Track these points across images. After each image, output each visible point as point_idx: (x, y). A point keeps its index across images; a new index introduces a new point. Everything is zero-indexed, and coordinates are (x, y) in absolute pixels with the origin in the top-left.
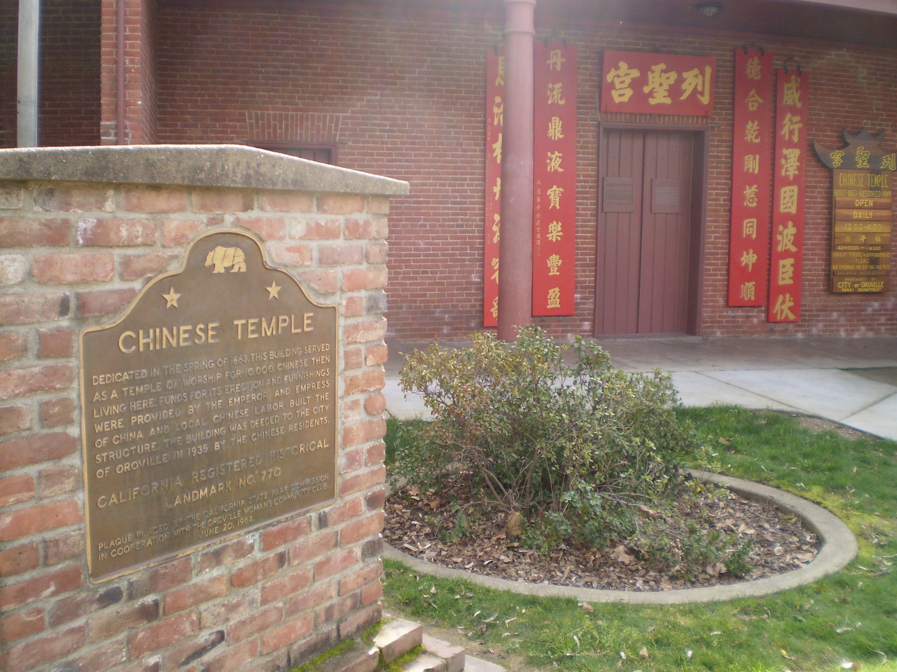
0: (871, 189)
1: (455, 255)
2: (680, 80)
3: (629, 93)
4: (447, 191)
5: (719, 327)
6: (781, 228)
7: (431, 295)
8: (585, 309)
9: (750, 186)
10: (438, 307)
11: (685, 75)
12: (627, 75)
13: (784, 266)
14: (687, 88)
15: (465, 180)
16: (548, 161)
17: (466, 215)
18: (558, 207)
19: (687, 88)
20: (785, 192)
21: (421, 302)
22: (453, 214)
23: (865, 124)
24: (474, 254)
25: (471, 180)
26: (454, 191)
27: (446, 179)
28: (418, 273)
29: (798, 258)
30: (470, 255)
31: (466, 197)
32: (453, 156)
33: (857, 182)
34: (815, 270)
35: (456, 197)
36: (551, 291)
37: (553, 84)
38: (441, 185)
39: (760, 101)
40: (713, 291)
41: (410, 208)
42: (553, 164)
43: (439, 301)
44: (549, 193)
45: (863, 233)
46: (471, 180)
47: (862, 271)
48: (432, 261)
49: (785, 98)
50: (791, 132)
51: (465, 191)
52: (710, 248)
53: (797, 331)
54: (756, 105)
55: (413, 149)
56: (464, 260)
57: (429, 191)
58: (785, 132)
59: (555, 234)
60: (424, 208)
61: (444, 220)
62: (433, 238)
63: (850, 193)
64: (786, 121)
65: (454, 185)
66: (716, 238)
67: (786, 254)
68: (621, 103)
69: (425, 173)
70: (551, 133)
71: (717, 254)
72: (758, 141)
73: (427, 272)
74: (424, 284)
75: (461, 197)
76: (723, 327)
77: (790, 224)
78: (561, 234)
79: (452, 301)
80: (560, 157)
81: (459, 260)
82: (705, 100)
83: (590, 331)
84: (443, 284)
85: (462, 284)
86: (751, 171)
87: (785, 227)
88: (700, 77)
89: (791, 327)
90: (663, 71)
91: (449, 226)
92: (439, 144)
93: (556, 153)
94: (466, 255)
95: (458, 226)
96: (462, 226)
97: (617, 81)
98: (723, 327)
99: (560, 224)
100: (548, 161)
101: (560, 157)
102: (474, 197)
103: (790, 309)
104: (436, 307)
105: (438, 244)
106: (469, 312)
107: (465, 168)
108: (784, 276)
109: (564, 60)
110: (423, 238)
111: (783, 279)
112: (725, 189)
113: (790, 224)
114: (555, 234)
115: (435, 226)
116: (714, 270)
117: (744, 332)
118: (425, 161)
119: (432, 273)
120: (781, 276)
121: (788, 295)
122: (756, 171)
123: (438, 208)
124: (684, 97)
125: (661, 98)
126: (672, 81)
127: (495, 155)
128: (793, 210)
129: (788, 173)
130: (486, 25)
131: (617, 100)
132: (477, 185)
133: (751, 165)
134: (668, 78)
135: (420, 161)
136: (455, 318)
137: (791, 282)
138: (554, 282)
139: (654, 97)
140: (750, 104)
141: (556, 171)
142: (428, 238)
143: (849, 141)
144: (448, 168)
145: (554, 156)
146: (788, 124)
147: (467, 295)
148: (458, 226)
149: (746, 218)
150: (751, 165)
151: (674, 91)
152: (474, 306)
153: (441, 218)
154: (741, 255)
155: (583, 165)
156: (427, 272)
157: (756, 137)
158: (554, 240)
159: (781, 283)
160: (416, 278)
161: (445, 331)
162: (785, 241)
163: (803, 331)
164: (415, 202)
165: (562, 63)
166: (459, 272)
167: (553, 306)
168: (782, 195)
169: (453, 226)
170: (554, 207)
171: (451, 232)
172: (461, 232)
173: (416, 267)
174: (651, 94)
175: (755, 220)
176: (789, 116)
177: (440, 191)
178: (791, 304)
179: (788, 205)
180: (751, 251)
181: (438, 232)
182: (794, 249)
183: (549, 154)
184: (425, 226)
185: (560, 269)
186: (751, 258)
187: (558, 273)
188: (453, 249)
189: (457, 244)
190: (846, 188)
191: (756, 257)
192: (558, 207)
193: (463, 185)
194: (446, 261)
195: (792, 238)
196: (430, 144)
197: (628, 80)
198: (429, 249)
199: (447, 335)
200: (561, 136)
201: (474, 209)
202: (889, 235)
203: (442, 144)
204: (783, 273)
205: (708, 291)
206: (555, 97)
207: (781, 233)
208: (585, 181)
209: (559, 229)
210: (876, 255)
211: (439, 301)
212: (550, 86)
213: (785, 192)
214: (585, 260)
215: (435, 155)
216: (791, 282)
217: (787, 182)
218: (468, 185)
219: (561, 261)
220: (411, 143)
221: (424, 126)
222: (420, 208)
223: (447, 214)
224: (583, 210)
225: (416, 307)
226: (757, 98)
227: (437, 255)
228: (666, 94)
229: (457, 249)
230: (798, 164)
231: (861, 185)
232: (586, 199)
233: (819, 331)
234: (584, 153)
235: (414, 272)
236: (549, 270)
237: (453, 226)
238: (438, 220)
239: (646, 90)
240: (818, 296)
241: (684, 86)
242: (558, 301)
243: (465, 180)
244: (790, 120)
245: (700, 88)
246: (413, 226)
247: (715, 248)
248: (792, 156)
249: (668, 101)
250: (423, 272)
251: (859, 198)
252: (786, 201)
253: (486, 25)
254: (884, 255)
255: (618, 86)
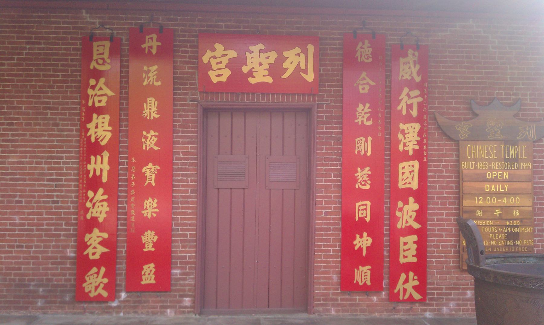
0: (506, 160)
1: (50, 230)
2: (281, 59)
3: (227, 73)
4: (43, 169)
5: (333, 305)
6: (400, 204)
7: (26, 269)
8: (185, 285)
9: (362, 169)
10: (33, 280)
11: (285, 54)
12: (223, 56)
13: (405, 244)
14: (290, 67)
15: (62, 158)
16: (143, 140)
17: (62, 191)
18: (154, 184)
19: (290, 67)
20: (404, 168)
21: (15, 275)
22: (48, 191)
23: (497, 94)
24: (70, 230)
25: (67, 158)
26: (49, 169)
27: (43, 158)
28: (13, 247)
29: (422, 236)
30: (65, 230)
31: (61, 175)
32: (49, 135)
33: (488, 154)
34: (443, 246)
35: (51, 175)
36: (145, 267)
37: (148, 67)
38: (37, 163)
39: (373, 83)
40: (325, 267)
41: (6, 185)
42: (148, 143)
43: (34, 275)
44: (144, 170)
45: (497, 207)
46: (67, 158)
47: (499, 247)
48: (27, 235)
49: (401, 73)
50: (410, 107)
51: (61, 169)
52: (321, 224)
53: (425, 311)
54: (367, 87)
55: (11, 130)
56: (60, 235)
57: (25, 168)
58: (402, 107)
59: (150, 210)
60: (20, 185)
61: (39, 196)
62: (29, 214)
63: (481, 165)
64: (403, 95)
65: (50, 163)
66: (326, 213)
67: (410, 231)
68: (219, 83)
69: (21, 152)
70: (146, 113)
71: (330, 230)
72: (370, 123)
73: (22, 247)
74: (19, 258)
75: (57, 174)
76: (339, 305)
77: (411, 200)
78: (157, 210)
79: (46, 275)
80: (155, 136)
81: (54, 235)
82: (310, 77)
83: (191, 307)
84: (37, 258)
85: (56, 258)
86: (362, 153)
87: (406, 203)
88: (302, 55)
89: (417, 306)
90: (261, 51)
91: (44, 202)
92: (36, 125)
93: (152, 133)
94: (62, 230)
95: (54, 202)
96: (57, 202)
97: (213, 62)
98: (339, 305)
99: (156, 201)
100: (143, 140)
101: (155, 136)
102: (70, 174)
103: (414, 287)
104: (29, 280)
105: (33, 219)
106: (62, 286)
107: (62, 147)
108: (406, 253)
109: (159, 44)
110: (17, 213)
111: (405, 257)
112: (335, 165)
113: (411, 200)
114: (150, 210)
115: (30, 202)
116: (325, 246)
117: (362, 311)
118: (22, 141)
119: (27, 247)
120: (402, 254)
121: (411, 274)
122: (369, 154)
123: (34, 185)
124: (285, 76)
125: (261, 77)
126: (272, 61)
127: (89, 134)
128: (415, 186)
129: (406, 149)
130: (84, 14)
131: (215, 80)
132: (73, 163)
133: (363, 147)
134: (267, 58)
135: (17, 141)
136: (50, 291)
137: (415, 260)
138: (149, 258)
139: (253, 77)
140: (361, 87)
141: (152, 149)
142: (24, 213)
143: (477, 112)
144: (43, 147)
145: (149, 135)
146: (406, 98)
147: (62, 269)
148: (54, 202)
149: (358, 201)
150: (363, 147)
151: (275, 69)
152: (70, 280)
153: (36, 194)
154: (355, 239)
155: (183, 143)
156: (22, 247)
157: (368, 120)
158: (149, 217)
159: (402, 260)
160: (11, 252)
161: (39, 304)
162: (405, 217)
163: (430, 311)
164: (11, 180)
165: (158, 47)
166: (54, 247)
167: (148, 282)
168: (400, 171)
169: (48, 202)
170: (150, 184)
171: (46, 208)
172: (57, 208)
173: (11, 241)
174: (250, 74)
175: (369, 203)
176: (406, 90)
177: (36, 168)
178: (416, 283)
179: (408, 181)
180: (365, 234)
181: (33, 208)
182: (416, 226)
183: (144, 133)
184: (21, 202)
185: (155, 245)
186: (365, 242)
187: (153, 249)
188: (48, 225)
189: (52, 219)
190: (476, 160)
191: (370, 240)
192: (154, 184)
193: (59, 163)
194: (41, 236)
195: (414, 215)
196: (27, 124)
197: (225, 61)
198: (23, 225)
199: (41, 308)
200: (157, 116)
201: (70, 186)
202: (531, 209)
203: (39, 125)
204: (404, 251)
205: (320, 267)
206: (151, 79)
207: (401, 210)
208: (184, 159)
209: (155, 205)
210: (515, 230)
211: (34, 275)
212: (146, 68)
213: (404, 168)
214: (186, 235)
215: (31, 135)
216: (415, 260)
217: (132, 209)
218: (64, 163)
219: (156, 237)
220: (8, 124)
221: (21, 108)
222: (16, 185)
223: (43, 191)
224: (183, 186)
225: (11, 280)
226: (368, 80)
227: (32, 230)
228: (267, 73)
229: (52, 225)
230: (419, 139)
231: (493, 156)
232: (186, 175)
233: (451, 310)
234: (183, 132)
235: (9, 246)
236: (143, 246)
237: (48, 202)
238: (34, 197)
239: (245, 69)
240: (449, 273)
241: (285, 65)
242: (153, 277)
243: (62, 158)
244: (408, 95)
245: (303, 66)
246: (9, 202)
247: (326, 224)
248: (411, 130)
249: (270, 80)
250: (18, 247)
251: (491, 169)
252: (405, 177)
253: (84, 14)
254: (524, 229)
255: (214, 66)
